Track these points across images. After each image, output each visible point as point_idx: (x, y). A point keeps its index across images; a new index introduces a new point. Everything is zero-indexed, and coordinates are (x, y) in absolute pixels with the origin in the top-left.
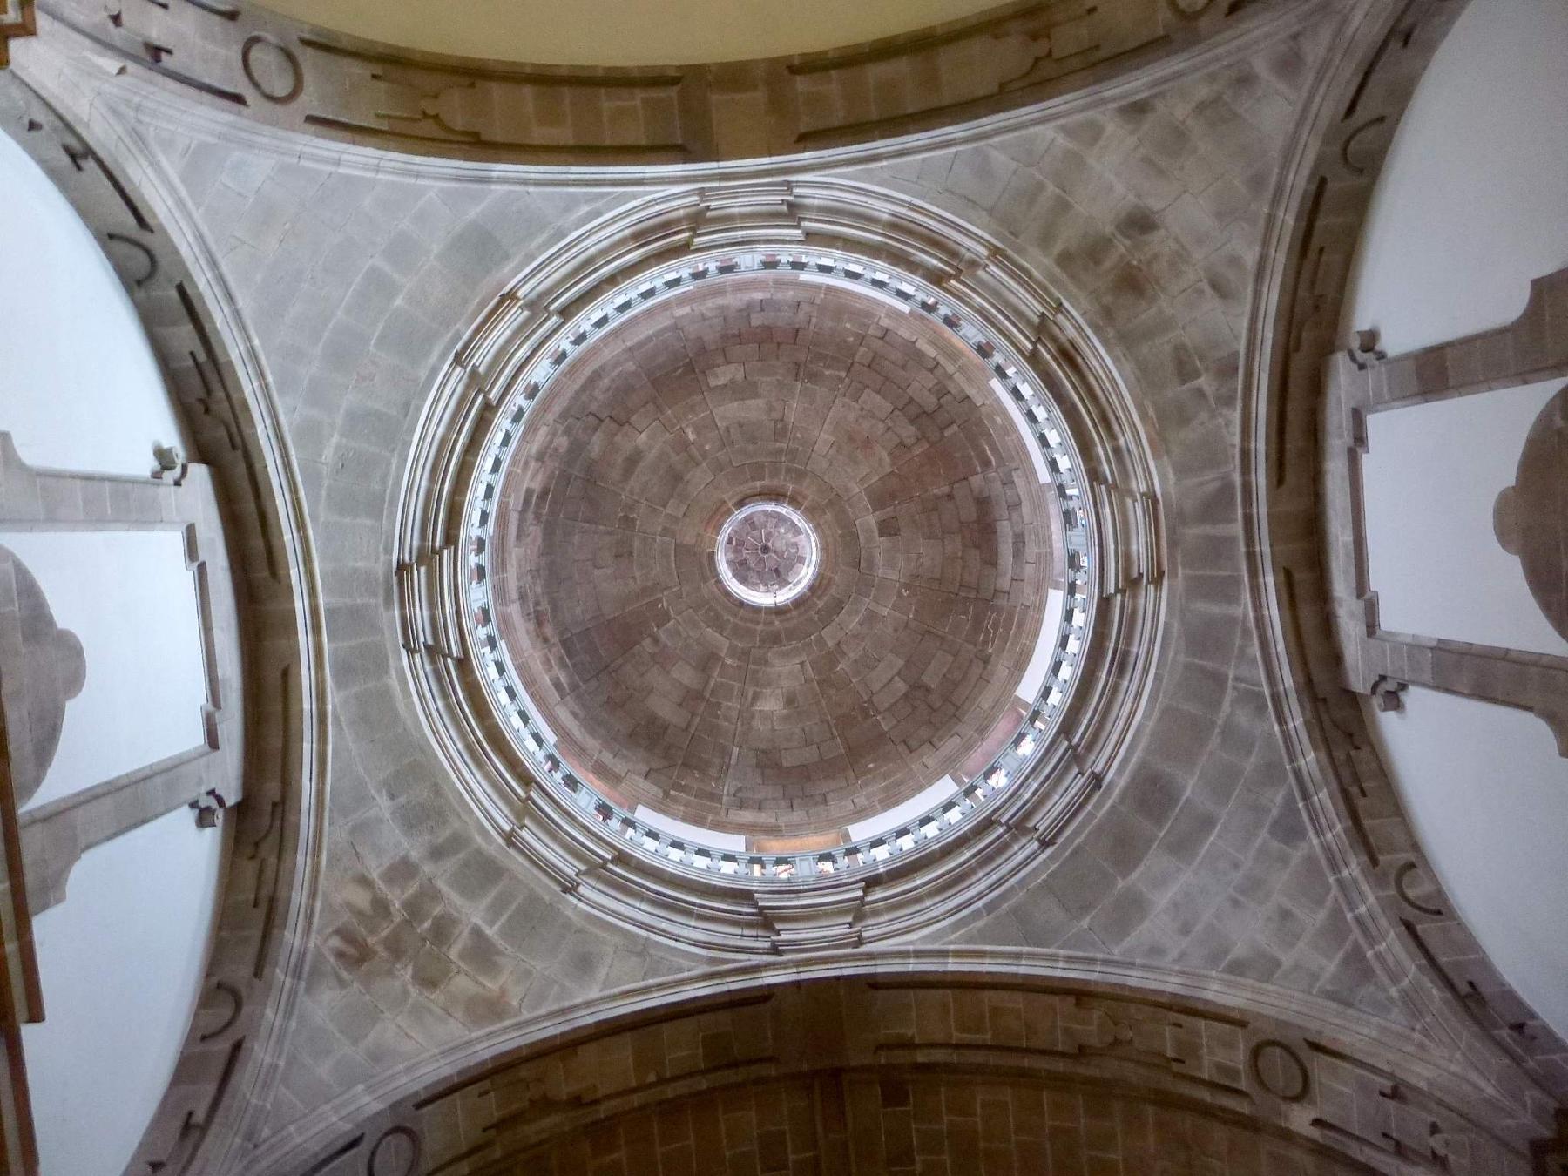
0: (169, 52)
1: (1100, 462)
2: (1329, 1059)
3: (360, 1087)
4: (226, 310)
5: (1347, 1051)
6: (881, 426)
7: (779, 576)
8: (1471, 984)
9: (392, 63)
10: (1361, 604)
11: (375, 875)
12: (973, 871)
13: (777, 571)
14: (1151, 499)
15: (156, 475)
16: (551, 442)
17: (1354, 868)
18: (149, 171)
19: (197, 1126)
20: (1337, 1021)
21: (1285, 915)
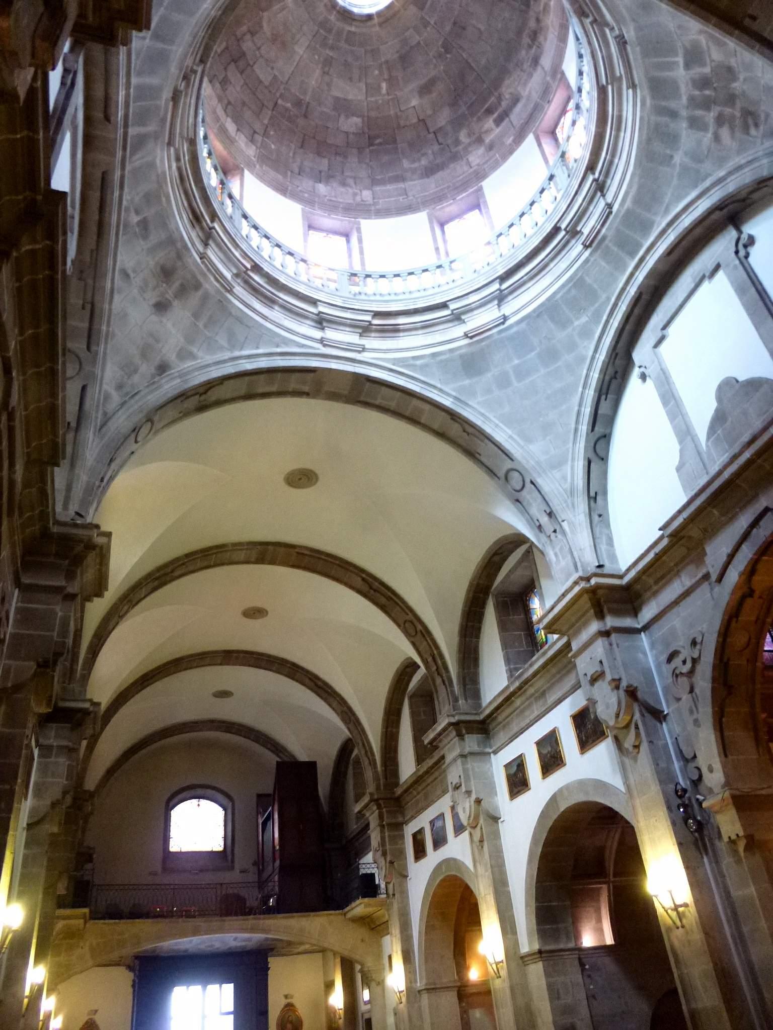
1: (188, 150)
6: (263, 51)
9: (471, 454)
11: (710, 135)
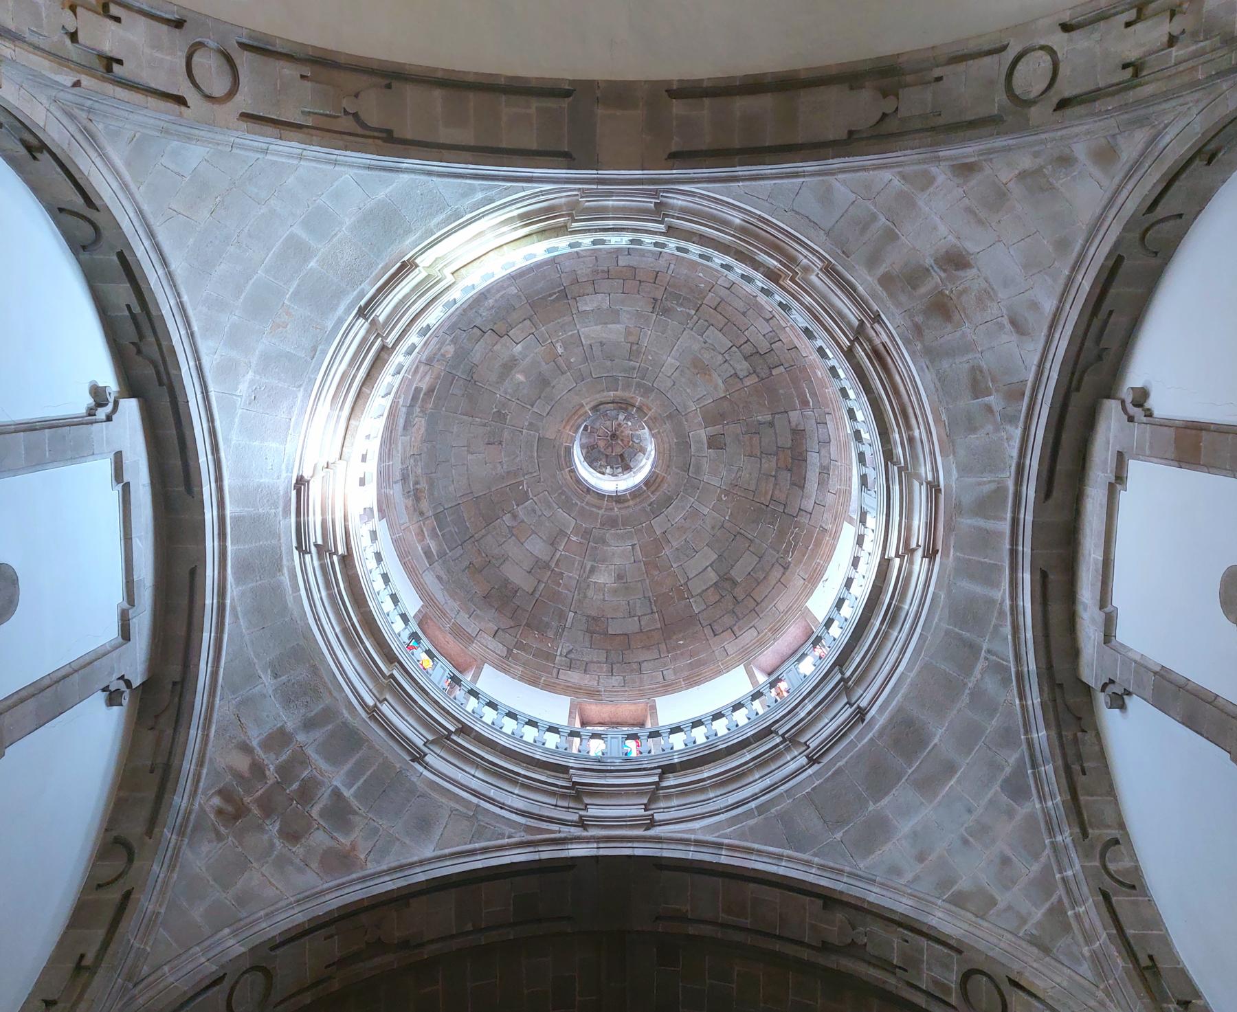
0: (120, 62)
2: (1026, 997)
3: (227, 931)
4: (160, 272)
5: (1040, 995)
7: (623, 464)
8: (1151, 957)
9: (320, 63)
10: (1103, 615)
11: (255, 743)
12: (750, 771)
13: (621, 456)
14: (934, 488)
15: (91, 412)
16: (440, 349)
17: (1065, 837)
18: (98, 162)
19: (87, 968)
20: (1035, 965)
21: (1006, 861)
